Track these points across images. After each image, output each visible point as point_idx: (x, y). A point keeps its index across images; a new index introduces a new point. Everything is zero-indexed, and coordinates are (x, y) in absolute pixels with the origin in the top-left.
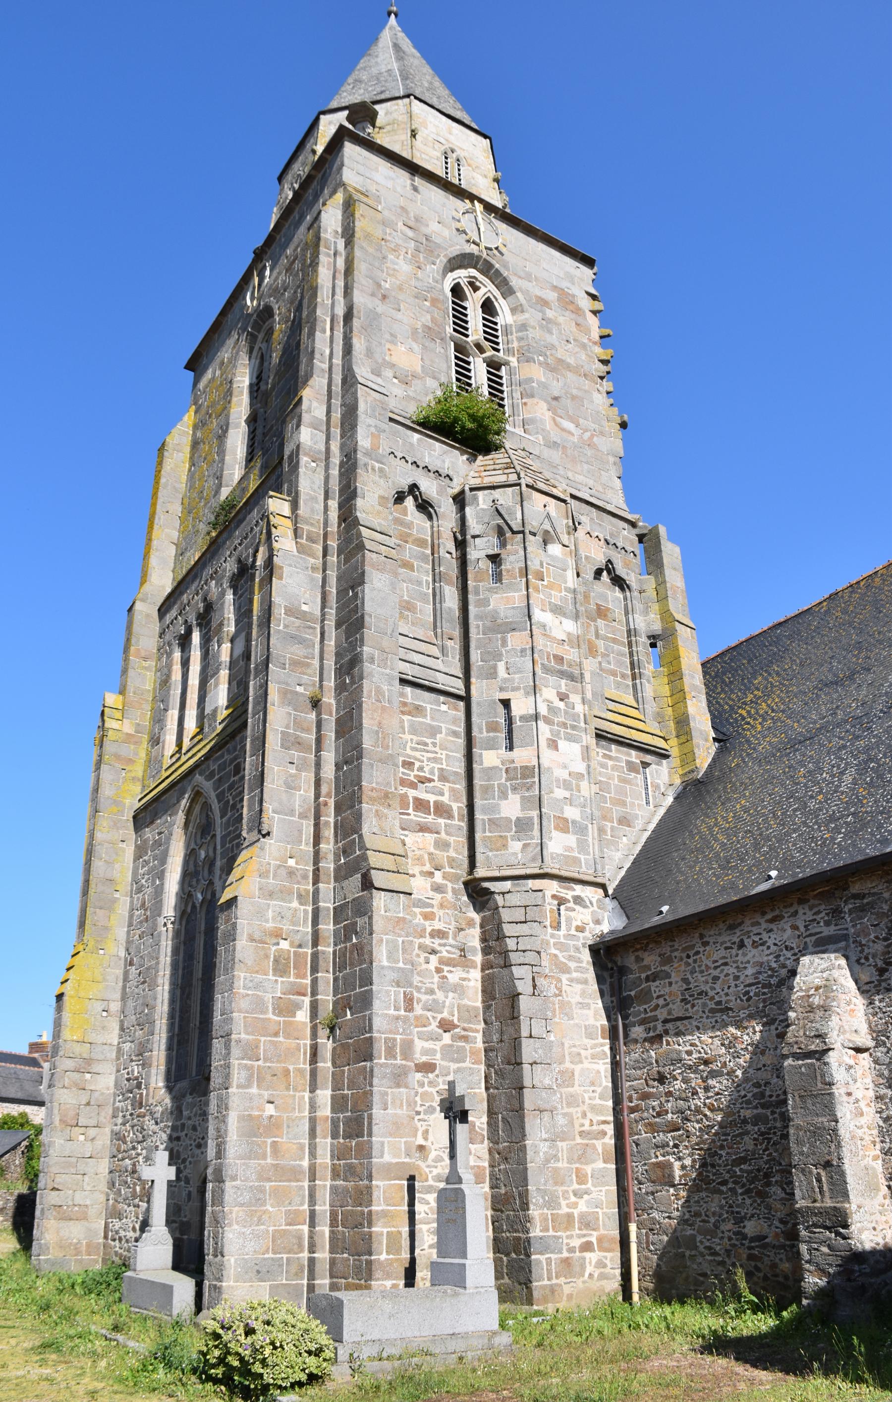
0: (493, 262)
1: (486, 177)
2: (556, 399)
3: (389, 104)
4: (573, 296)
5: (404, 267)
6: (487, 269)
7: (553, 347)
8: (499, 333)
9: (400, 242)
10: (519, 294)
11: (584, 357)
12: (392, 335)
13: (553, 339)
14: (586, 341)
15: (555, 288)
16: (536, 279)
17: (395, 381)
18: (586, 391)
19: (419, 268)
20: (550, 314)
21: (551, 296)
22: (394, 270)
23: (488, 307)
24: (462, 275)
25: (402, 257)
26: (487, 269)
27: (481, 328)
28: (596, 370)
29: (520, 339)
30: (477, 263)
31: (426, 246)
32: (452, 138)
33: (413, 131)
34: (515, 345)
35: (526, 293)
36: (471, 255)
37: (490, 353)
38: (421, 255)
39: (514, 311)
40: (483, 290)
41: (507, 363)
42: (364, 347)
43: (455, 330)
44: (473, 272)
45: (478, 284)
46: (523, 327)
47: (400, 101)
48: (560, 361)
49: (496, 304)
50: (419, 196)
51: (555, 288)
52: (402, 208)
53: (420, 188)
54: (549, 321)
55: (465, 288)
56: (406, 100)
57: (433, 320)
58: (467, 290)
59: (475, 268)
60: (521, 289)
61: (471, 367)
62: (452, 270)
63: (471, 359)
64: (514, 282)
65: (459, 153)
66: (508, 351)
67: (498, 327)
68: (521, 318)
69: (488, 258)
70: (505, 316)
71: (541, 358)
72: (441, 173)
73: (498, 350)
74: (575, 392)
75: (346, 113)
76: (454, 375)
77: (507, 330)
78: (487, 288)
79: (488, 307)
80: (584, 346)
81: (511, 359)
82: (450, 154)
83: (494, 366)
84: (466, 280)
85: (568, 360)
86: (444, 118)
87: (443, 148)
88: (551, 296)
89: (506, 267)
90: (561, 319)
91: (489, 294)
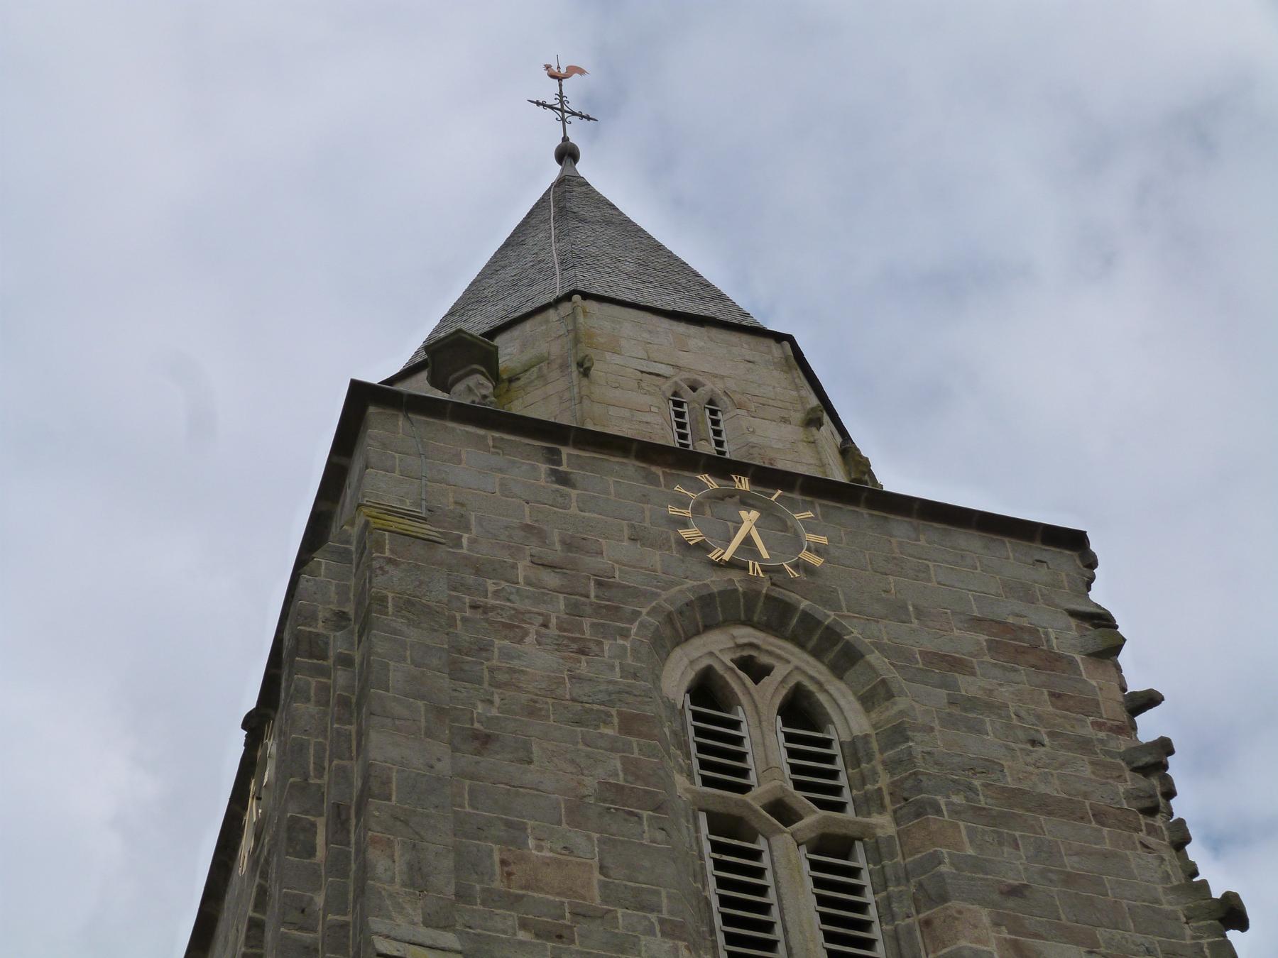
0: (793, 597)
1: (785, 420)
2: (1015, 892)
3: (528, 326)
4: (1033, 631)
5: (538, 660)
6: (778, 616)
7: (989, 766)
8: (839, 765)
9: (525, 605)
10: (874, 658)
11: (1087, 771)
12: (509, 825)
13: (988, 742)
14: (1088, 731)
15: (977, 623)
16: (920, 613)
17: (522, 935)
18: (1105, 856)
19: (582, 652)
20: (969, 686)
21: (967, 642)
22: (512, 671)
23: (799, 711)
24: (716, 648)
25: (531, 638)
26: (778, 616)
27: (782, 759)
28: (1130, 796)
29: (891, 766)
30: (750, 609)
31: (608, 602)
32: (685, 359)
33: (580, 365)
34: (884, 781)
35: (897, 653)
36: (728, 595)
37: (813, 819)
38: (586, 623)
39: (868, 701)
40: (780, 671)
41: (866, 834)
42: (400, 866)
43: (707, 782)
44: (745, 634)
45: (764, 659)
46: (897, 733)
47: (551, 313)
48: (1014, 796)
49: (821, 697)
50: (574, 493)
51: (977, 623)
52: (527, 528)
53: (577, 474)
54: (971, 704)
55: (729, 677)
56: (565, 308)
57: (631, 767)
58: (738, 682)
59: (748, 623)
60: (879, 646)
61: (765, 862)
62: (679, 641)
63: (761, 845)
64: (855, 633)
65: (710, 387)
66: (868, 803)
67: (836, 750)
68: (888, 713)
69: (777, 592)
70: (847, 718)
71: (956, 799)
72: (672, 440)
73: (840, 807)
74: (1071, 863)
75: (424, 375)
76: (713, 892)
77: (856, 752)
78: (792, 664)
79: (799, 711)
80: (1084, 745)
81: (876, 819)
82: (687, 395)
83: (831, 852)
84: (727, 659)
85: (1042, 788)
86: (665, 323)
87: (667, 387)
88: (967, 642)
89: (829, 600)
90: (1004, 693)
91: (798, 678)
